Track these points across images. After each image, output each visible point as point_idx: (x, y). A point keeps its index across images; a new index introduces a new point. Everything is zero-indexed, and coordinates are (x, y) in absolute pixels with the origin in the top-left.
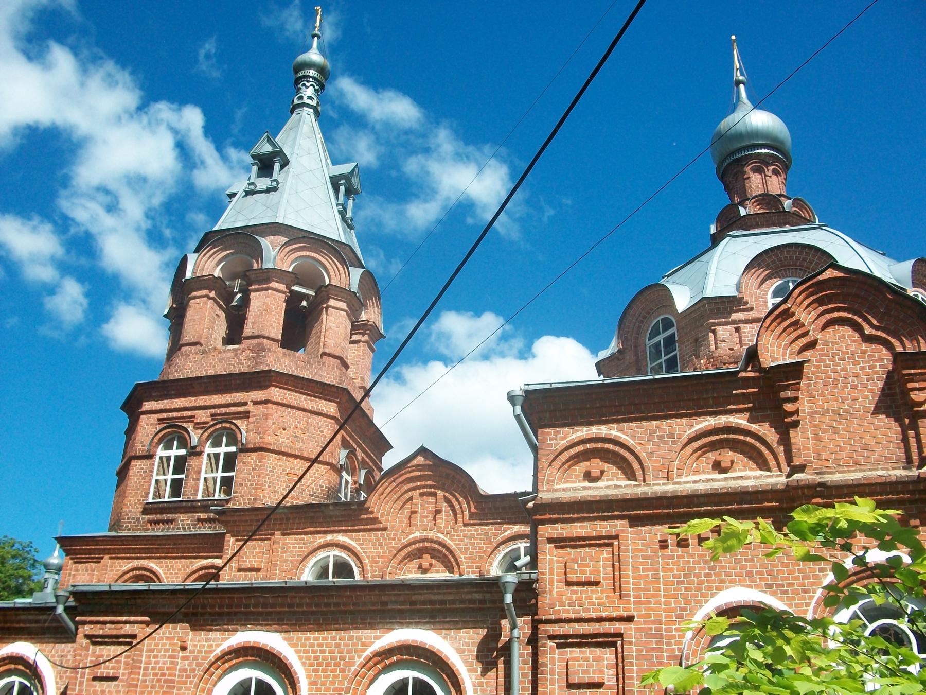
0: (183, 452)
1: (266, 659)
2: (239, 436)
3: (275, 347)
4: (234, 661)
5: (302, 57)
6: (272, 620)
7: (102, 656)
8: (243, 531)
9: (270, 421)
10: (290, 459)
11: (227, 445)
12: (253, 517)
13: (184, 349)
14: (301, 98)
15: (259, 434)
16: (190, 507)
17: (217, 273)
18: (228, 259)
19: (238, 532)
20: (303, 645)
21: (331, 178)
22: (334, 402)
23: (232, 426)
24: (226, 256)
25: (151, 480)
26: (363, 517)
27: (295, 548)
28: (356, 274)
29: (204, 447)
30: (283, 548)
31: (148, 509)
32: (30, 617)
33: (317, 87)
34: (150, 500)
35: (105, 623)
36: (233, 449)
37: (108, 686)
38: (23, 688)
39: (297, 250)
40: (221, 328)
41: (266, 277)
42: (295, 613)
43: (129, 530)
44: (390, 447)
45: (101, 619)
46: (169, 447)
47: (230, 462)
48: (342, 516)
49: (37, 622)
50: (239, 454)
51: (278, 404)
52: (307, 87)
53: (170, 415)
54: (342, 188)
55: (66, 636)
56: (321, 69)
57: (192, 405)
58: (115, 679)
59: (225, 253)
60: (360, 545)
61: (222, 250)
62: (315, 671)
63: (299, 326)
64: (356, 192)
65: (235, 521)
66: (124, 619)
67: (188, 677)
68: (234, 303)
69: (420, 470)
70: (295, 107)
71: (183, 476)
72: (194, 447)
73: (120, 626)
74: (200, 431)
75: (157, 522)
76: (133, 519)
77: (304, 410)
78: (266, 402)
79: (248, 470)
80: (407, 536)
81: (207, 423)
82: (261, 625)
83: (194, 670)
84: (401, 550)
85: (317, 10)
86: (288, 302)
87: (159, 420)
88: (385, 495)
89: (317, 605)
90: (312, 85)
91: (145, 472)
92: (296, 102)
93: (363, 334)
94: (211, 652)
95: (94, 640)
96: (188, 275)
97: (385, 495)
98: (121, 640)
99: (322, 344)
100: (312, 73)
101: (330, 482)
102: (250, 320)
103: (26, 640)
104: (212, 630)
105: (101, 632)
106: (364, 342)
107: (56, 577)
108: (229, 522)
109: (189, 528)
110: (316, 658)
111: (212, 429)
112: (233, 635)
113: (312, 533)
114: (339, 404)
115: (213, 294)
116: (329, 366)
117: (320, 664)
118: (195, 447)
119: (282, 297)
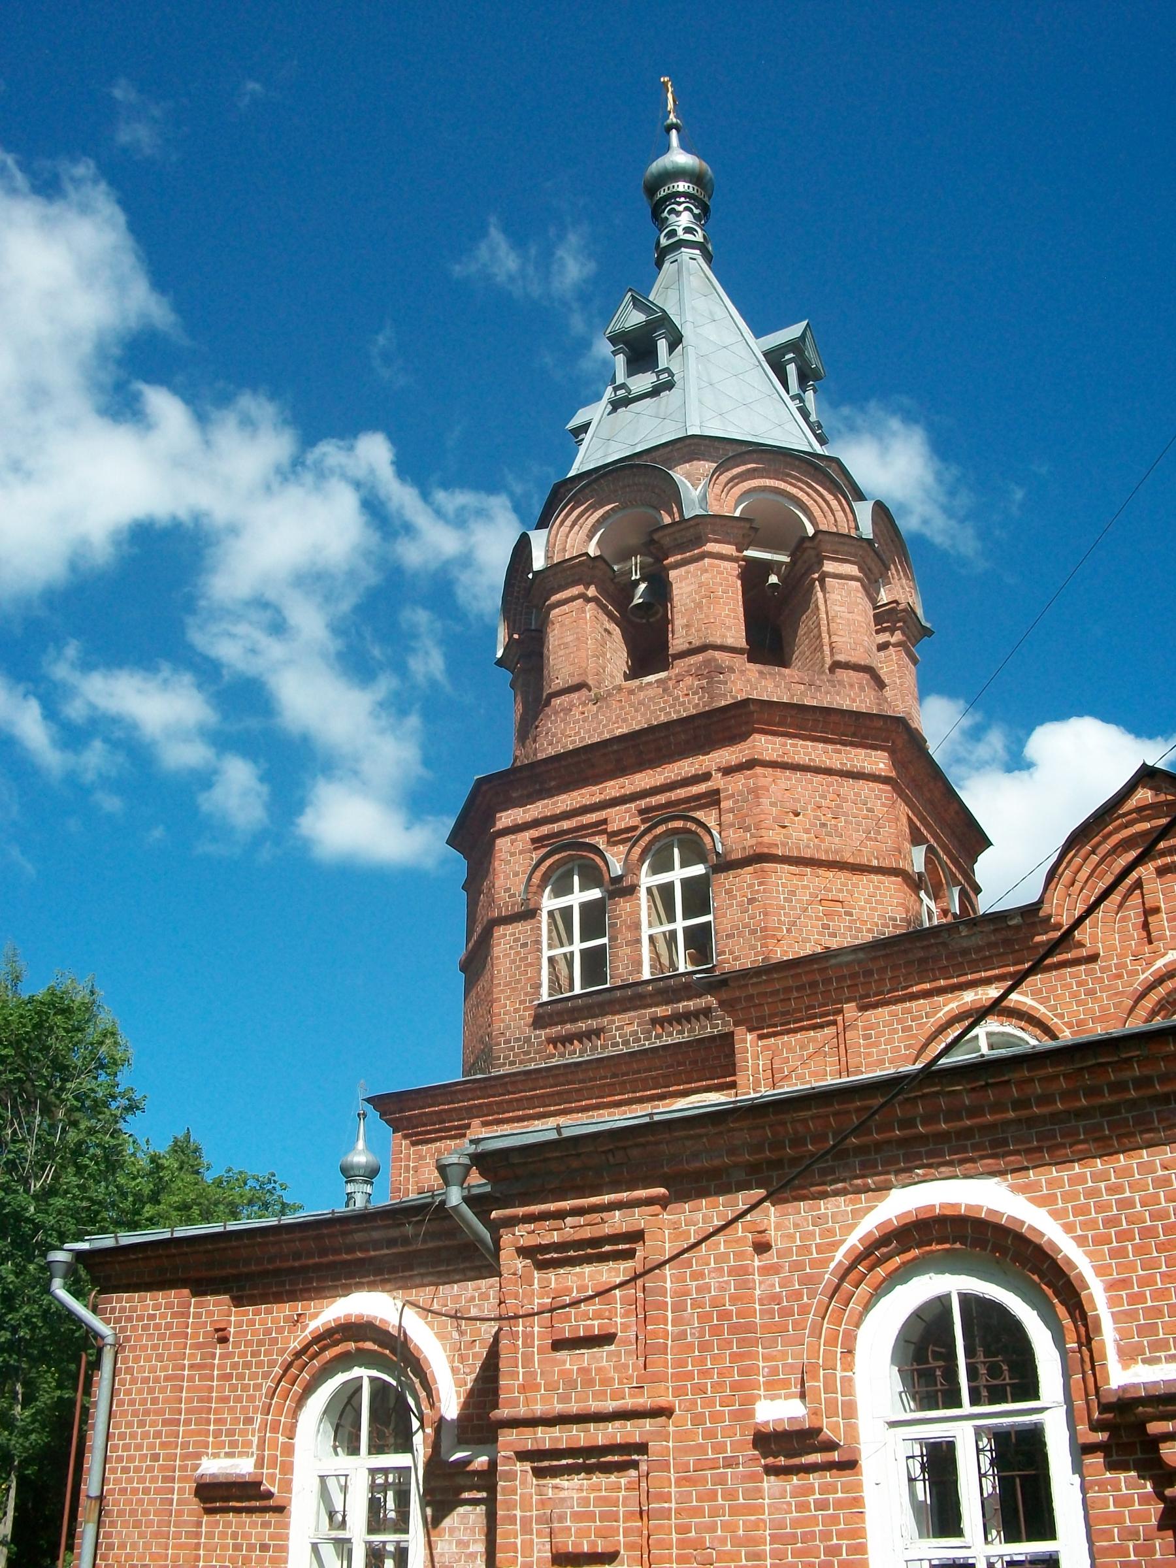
0: (595, 894)
1: (979, 1243)
2: (707, 839)
3: (740, 661)
4: (898, 1260)
5: (657, 165)
6: (975, 1147)
7: (568, 1291)
8: (772, 1016)
9: (765, 801)
10: (821, 871)
11: (683, 866)
12: (791, 983)
13: (556, 702)
14: (673, 233)
15: (747, 829)
16: (632, 997)
17: (592, 550)
18: (610, 521)
19: (762, 1019)
20: (1068, 1197)
21: (766, 354)
22: (883, 749)
23: (689, 825)
24: (604, 518)
25: (539, 958)
26: (1038, 939)
27: (895, 1031)
28: (864, 512)
29: (638, 876)
30: (867, 1037)
31: (543, 1017)
32: (376, 1235)
33: (696, 211)
34: (545, 998)
35: (560, 1215)
36: (698, 870)
37: (592, 1357)
38: (380, 1389)
39: (742, 477)
40: (617, 657)
41: (692, 535)
42: (1031, 1122)
43: (512, 1063)
44: (989, 844)
45: (552, 1207)
46: (563, 889)
47: (698, 896)
48: (991, 945)
49: (391, 1243)
50: (713, 877)
51: (774, 765)
52: (678, 214)
53: (555, 827)
54: (792, 369)
55: (477, 1261)
56: (696, 177)
57: (597, 799)
58: (606, 1339)
59: (601, 512)
60: (1044, 1001)
61: (594, 507)
62: (1114, 1254)
63: (774, 620)
64: (817, 377)
65: (750, 998)
66: (606, 1198)
67: (786, 1313)
68: (637, 600)
69: (1148, 819)
70: (662, 254)
71: (605, 940)
72: (618, 879)
73: (596, 1217)
74: (623, 849)
75: (567, 1039)
76: (517, 1040)
77: (828, 772)
78: (751, 764)
79: (740, 905)
80: (1150, 964)
81: (635, 828)
82: (950, 1163)
83: (798, 1295)
84: (1143, 996)
85: (665, 84)
86: (745, 576)
87: (534, 841)
88: (1078, 885)
89: (1091, 1092)
90: (687, 209)
91: (524, 945)
92: (664, 242)
93: (892, 631)
94: (835, 1246)
95: (543, 1258)
96: (538, 563)
97: (1078, 885)
98: (607, 1248)
99: (826, 649)
100: (682, 186)
101: (907, 912)
102: (679, 622)
103: (372, 1286)
104: (824, 1195)
105: (556, 1237)
106: (895, 645)
107: (368, 1189)
108: (737, 1000)
109: (638, 1040)
110: (1111, 1222)
111: (647, 838)
112: (881, 1200)
113: (927, 994)
114: (892, 752)
115: (592, 592)
116: (852, 686)
117: (1123, 1236)
118: (619, 879)
119: (733, 569)
